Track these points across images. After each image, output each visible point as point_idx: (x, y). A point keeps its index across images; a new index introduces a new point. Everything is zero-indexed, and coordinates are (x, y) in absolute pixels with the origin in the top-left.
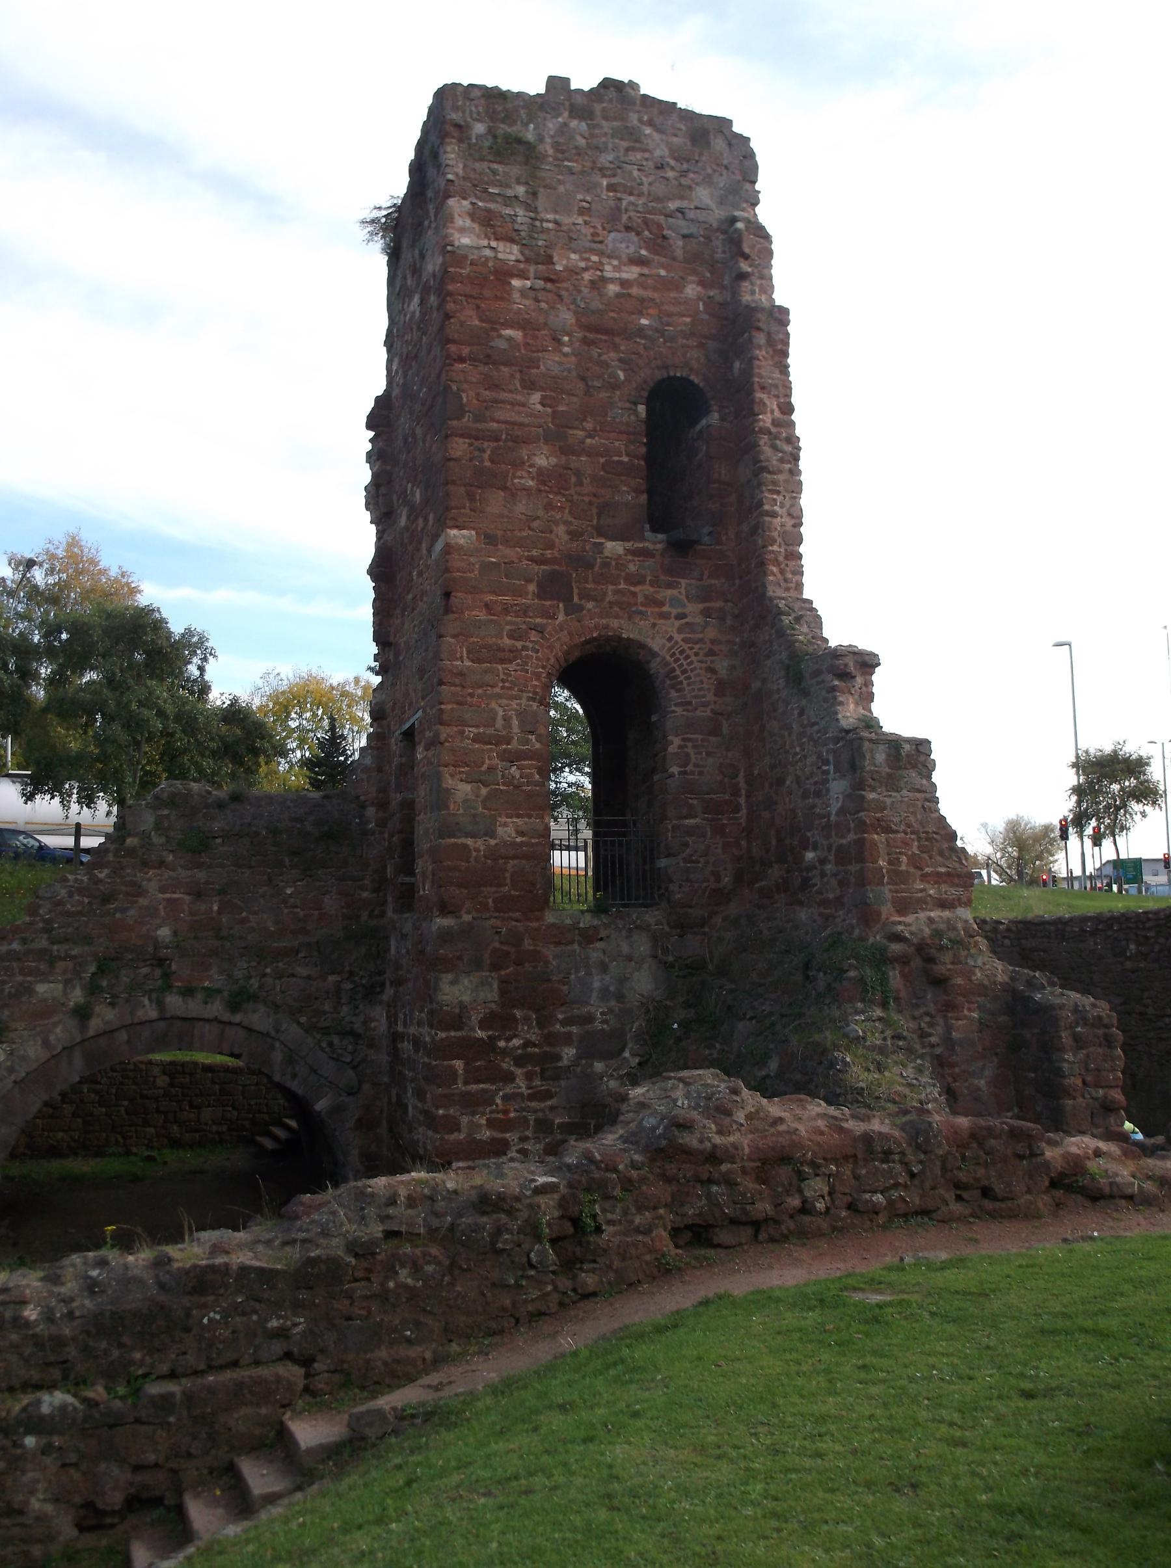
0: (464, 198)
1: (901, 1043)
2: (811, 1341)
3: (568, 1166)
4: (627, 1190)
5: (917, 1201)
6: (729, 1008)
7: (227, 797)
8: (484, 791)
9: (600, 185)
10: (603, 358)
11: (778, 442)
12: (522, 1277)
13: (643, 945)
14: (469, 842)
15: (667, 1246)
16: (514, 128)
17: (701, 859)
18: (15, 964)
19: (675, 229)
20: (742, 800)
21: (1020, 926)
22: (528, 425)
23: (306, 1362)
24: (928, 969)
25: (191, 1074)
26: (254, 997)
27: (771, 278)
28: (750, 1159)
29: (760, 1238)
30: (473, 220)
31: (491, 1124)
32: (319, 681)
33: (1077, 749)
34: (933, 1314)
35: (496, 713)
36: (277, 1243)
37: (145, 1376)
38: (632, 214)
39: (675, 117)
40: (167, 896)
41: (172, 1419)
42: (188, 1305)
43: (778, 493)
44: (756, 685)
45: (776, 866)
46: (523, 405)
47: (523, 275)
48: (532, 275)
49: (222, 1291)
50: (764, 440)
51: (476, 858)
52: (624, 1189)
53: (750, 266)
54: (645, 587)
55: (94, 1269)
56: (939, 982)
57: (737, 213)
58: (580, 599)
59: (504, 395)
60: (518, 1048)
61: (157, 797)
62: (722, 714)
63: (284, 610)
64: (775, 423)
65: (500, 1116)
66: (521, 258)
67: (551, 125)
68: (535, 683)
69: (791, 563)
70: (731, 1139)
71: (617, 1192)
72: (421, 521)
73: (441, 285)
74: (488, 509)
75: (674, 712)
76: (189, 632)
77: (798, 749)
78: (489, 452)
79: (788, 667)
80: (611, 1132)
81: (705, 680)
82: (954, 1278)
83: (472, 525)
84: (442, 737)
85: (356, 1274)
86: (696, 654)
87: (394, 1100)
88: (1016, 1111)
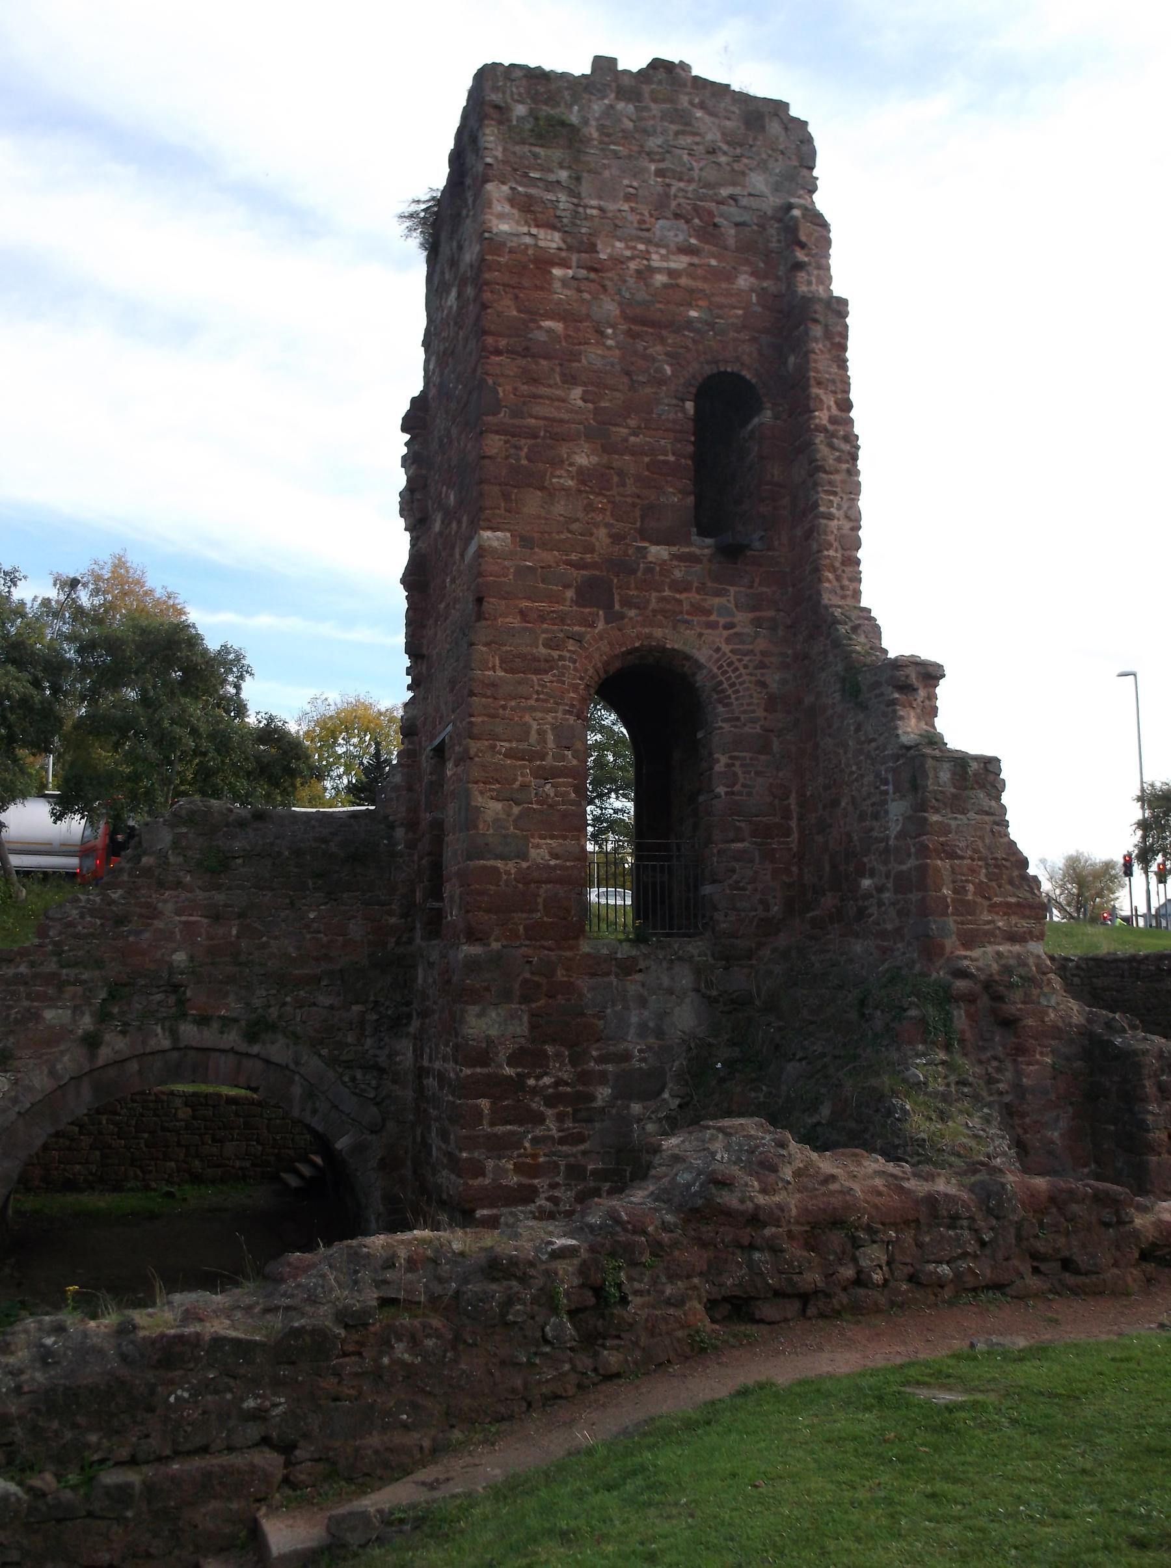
0: (503, 183)
1: (966, 1090)
2: (867, 1455)
3: (591, 1227)
4: (657, 1256)
5: (988, 1272)
6: (777, 1047)
7: (249, 816)
8: (516, 810)
9: (647, 170)
10: (650, 351)
11: (835, 441)
12: (536, 1354)
13: (685, 979)
14: (499, 864)
15: (700, 1321)
16: (558, 110)
17: (749, 887)
18: (22, 989)
19: (727, 219)
20: (793, 824)
21: (1091, 963)
22: (568, 422)
23: (286, 1449)
24: (997, 1008)
25: (214, 1106)
26: (273, 1028)
27: (828, 269)
28: (798, 1223)
29: (809, 1312)
30: (512, 206)
31: (518, 1168)
32: (368, 707)
33: (1142, 782)
34: (1014, 1422)
35: (530, 727)
36: (257, 1310)
37: (102, 1461)
38: (682, 201)
39: (728, 99)
40: (184, 918)
41: (129, 1514)
42: (153, 1381)
43: (835, 494)
44: (809, 700)
45: (829, 894)
46: (564, 401)
47: (564, 264)
48: (574, 264)
49: (192, 1365)
50: (820, 438)
51: (506, 881)
52: (653, 1254)
53: (807, 255)
54: (690, 595)
55: (49, 1336)
56: (1009, 1023)
57: (793, 200)
58: (622, 606)
59: (543, 390)
60: (549, 1087)
61: (175, 815)
62: (772, 731)
63: (318, 628)
64: (833, 420)
65: (529, 1160)
66: (563, 246)
67: (596, 107)
68: (572, 695)
69: (848, 569)
70: (777, 1199)
71: (646, 1258)
72: (454, 525)
73: (477, 276)
74: (525, 510)
75: (721, 728)
76: (225, 649)
77: (854, 768)
78: (526, 450)
79: (844, 680)
80: (640, 1188)
81: (755, 694)
82: (1031, 1373)
83: (507, 526)
84: (472, 752)
85: (345, 1348)
86: (746, 667)
87: (419, 1139)
88: (1093, 1166)
